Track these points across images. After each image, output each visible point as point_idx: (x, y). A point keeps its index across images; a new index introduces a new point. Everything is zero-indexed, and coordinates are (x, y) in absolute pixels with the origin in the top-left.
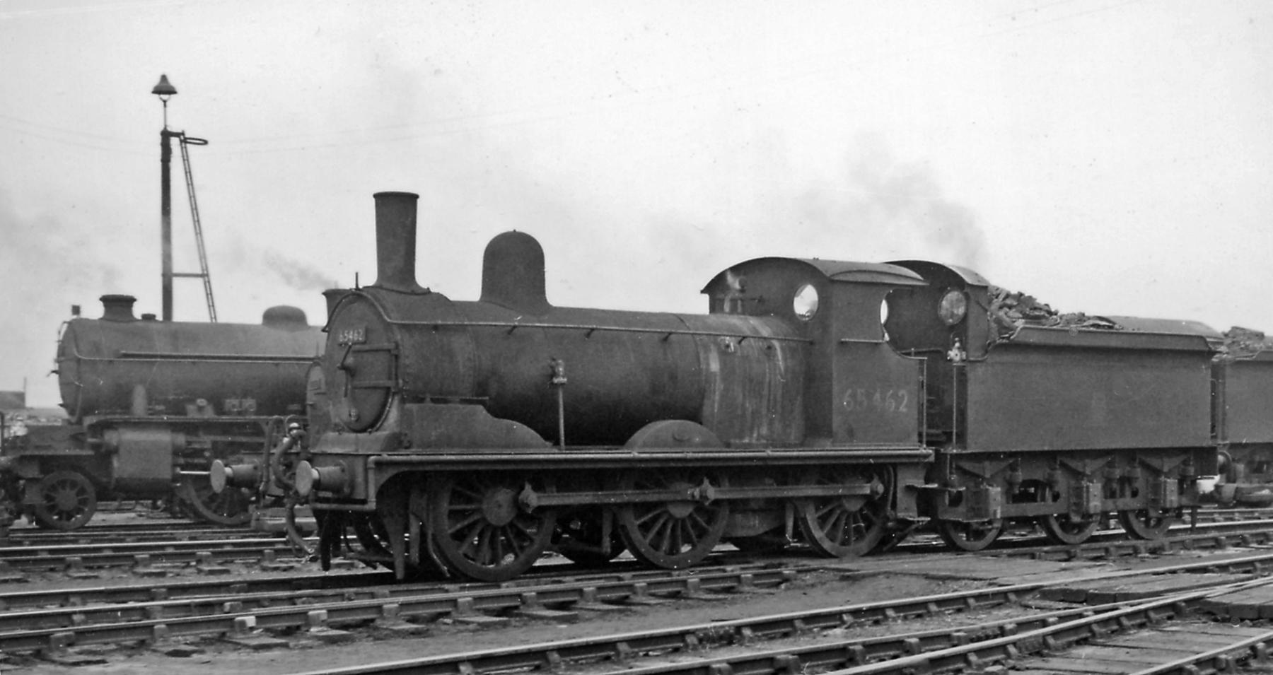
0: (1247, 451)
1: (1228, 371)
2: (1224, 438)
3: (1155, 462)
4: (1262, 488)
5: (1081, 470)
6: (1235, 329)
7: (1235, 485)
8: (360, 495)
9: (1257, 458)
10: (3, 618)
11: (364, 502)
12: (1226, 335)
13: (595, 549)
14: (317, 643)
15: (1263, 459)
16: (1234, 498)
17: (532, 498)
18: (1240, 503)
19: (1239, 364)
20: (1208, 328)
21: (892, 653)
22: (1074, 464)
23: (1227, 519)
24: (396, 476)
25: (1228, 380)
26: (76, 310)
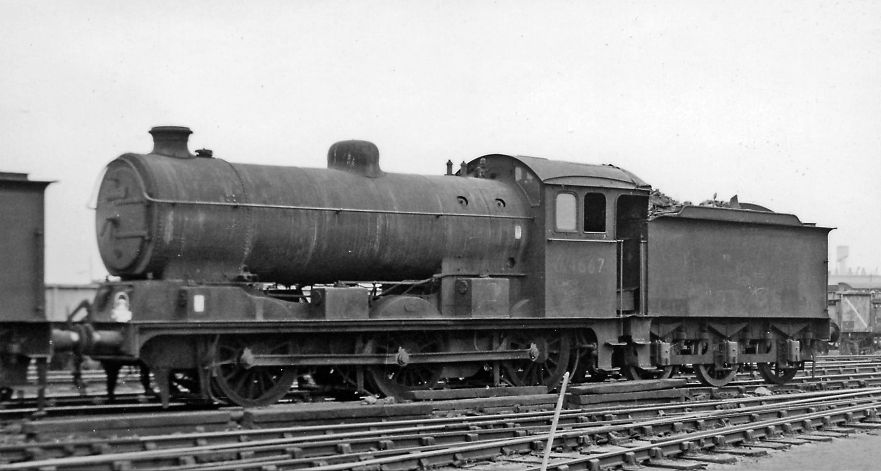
0: (738, 328)
3: (721, 329)
5: (724, 333)
17: (249, 357)
22: (778, 326)
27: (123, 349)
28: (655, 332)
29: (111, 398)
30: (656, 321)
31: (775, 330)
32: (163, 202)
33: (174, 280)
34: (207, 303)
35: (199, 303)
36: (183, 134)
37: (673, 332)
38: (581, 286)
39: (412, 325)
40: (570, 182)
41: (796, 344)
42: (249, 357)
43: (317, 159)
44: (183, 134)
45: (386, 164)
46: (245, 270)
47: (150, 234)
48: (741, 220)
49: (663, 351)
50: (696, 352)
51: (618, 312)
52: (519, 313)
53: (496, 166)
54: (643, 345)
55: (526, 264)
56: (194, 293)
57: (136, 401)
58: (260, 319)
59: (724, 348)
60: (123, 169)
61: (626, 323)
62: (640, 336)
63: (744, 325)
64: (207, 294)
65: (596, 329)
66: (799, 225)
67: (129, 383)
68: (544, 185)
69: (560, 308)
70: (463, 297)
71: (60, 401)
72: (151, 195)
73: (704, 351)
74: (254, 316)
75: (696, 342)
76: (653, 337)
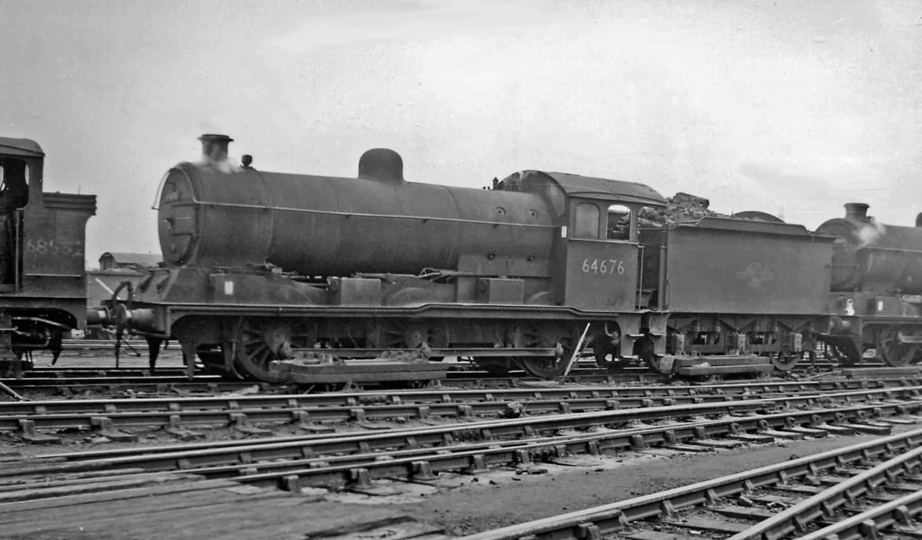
0: (689, 321)
1: (671, 237)
2: (665, 308)
3: (730, 322)
4: (701, 361)
5: (790, 326)
6: (680, 195)
7: (674, 357)
8: (162, 329)
9: (698, 329)
10: (2, 298)
11: (163, 333)
12: (671, 201)
13: (222, 367)
14: (203, 477)
15: (705, 330)
16: (673, 370)
17: (903, 338)
18: (679, 377)
19: (682, 230)
20: (659, 195)
21: (293, 455)
22: (784, 322)
23: (706, 400)
24: (186, 316)
25: (670, 246)
26: (217, 144)
27: (153, 325)
28: (672, 326)
29: (152, 370)
30: (674, 315)
31: (780, 324)
32: (214, 203)
33: (867, 293)
34: (236, 288)
35: (880, 306)
36: (864, 207)
37: (687, 326)
38: (598, 284)
39: (355, 313)
40: (578, 195)
41: (799, 336)
42: (903, 338)
43: (349, 169)
44: (864, 207)
45: (410, 174)
46: (268, 261)
47: (197, 231)
48: (782, 232)
49: (739, 342)
50: (766, 342)
51: (637, 307)
52: (538, 304)
53: (536, 181)
54: (659, 336)
55: (552, 261)
56: (878, 301)
57: (141, 374)
58: (904, 316)
59: (790, 340)
60: (179, 175)
61: (644, 318)
62: (658, 329)
63: (753, 319)
64: (884, 301)
65: (618, 321)
66: (805, 234)
67: (172, 359)
68: (569, 197)
69: (580, 300)
70: (480, 291)
71: (868, 360)
72: (198, 200)
73: (716, 342)
74: (901, 314)
75: (767, 334)
76: (670, 330)
